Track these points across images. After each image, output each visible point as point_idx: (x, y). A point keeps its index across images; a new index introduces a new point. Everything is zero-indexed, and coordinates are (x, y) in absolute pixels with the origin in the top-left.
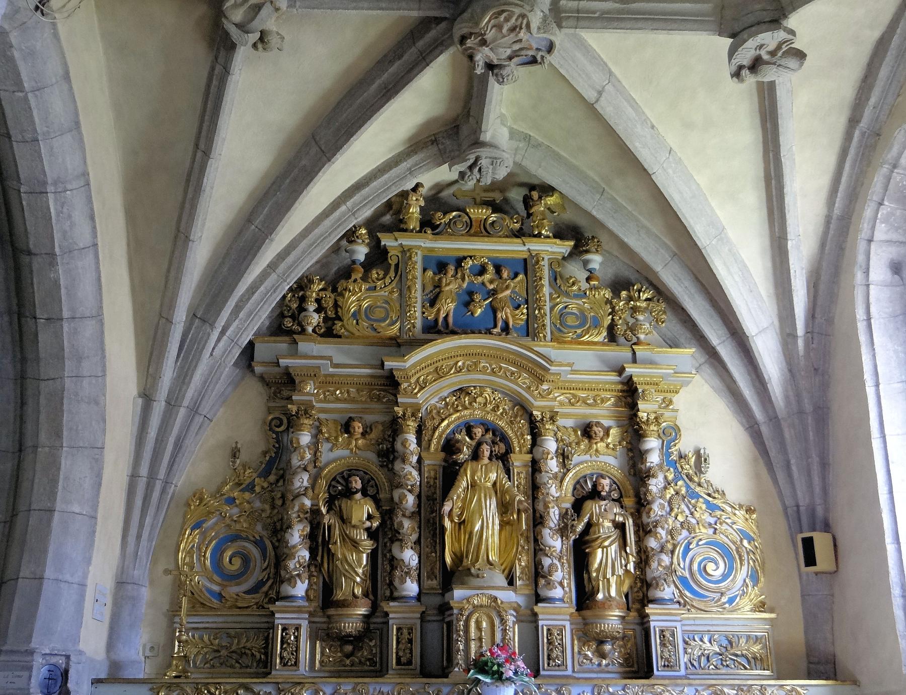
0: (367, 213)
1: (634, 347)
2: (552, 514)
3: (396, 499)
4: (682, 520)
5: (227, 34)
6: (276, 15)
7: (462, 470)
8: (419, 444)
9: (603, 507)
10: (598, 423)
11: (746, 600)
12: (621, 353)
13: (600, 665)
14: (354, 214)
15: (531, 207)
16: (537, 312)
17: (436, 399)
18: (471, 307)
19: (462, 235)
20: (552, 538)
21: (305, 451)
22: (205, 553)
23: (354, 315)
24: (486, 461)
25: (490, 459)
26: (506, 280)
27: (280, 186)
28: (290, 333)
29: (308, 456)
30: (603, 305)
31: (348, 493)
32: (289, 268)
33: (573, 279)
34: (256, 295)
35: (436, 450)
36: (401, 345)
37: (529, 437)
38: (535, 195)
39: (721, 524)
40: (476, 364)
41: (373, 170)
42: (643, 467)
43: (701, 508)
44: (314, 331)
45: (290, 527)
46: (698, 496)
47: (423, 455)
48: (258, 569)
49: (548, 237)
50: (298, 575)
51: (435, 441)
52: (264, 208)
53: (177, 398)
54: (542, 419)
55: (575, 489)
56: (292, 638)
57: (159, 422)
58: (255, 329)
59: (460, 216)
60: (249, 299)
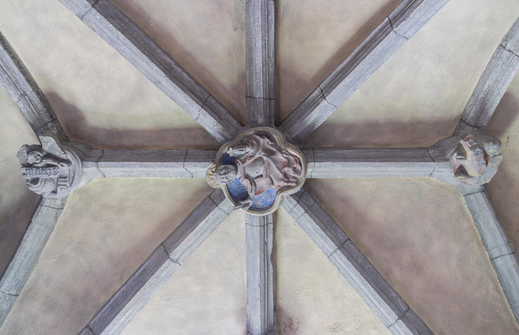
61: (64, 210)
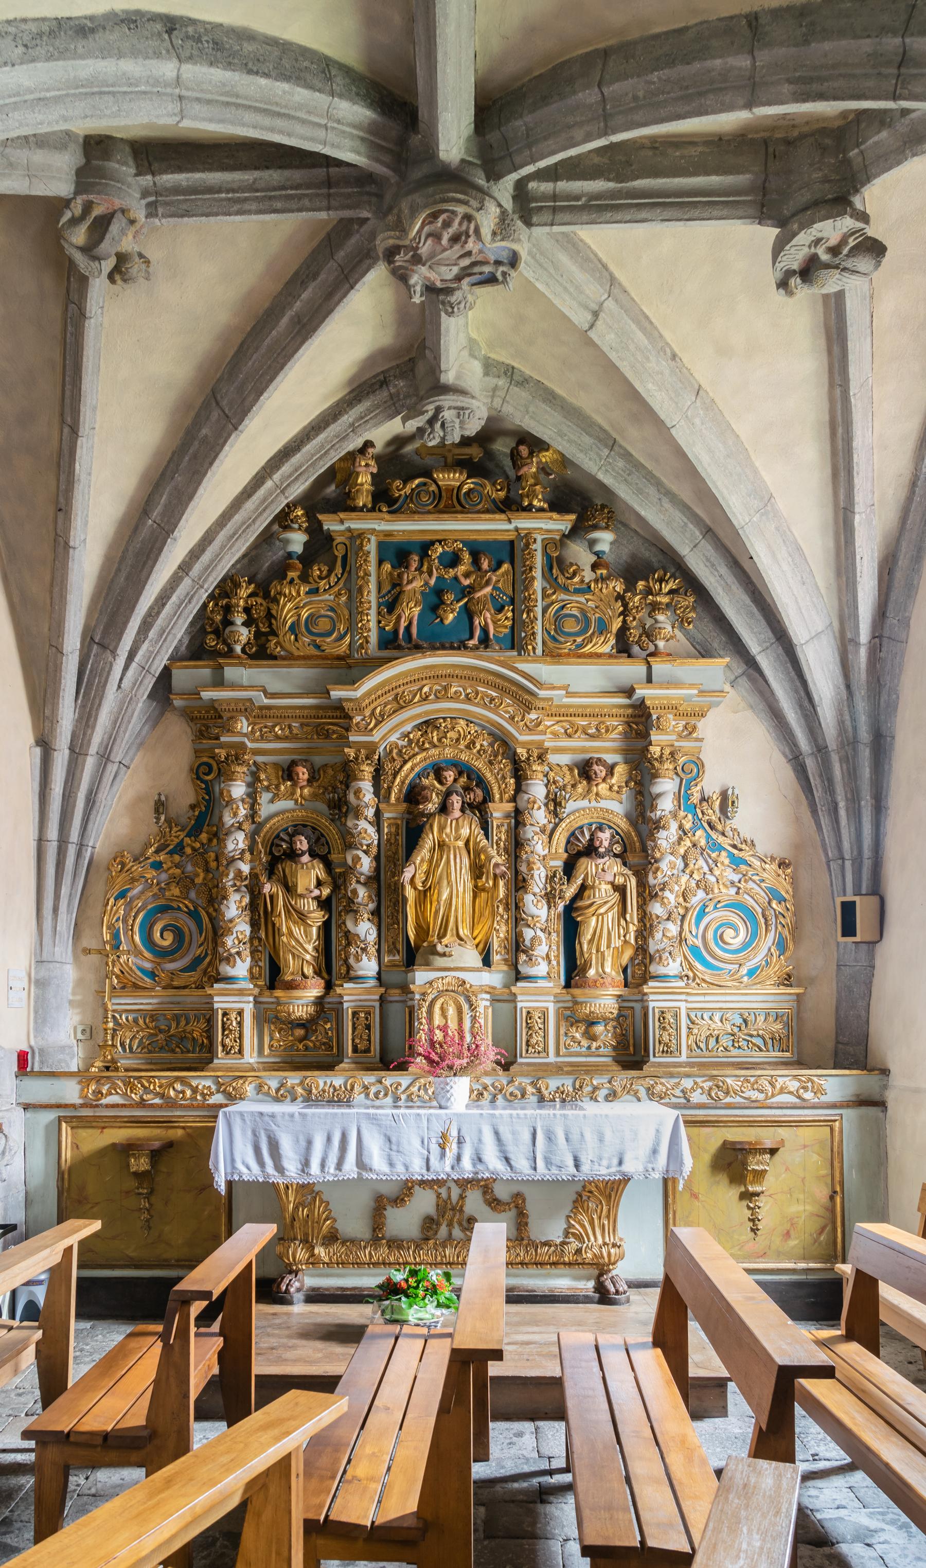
0: (298, 490)
1: (649, 659)
2: (536, 877)
3: (350, 862)
4: (697, 878)
5: (71, 263)
6: (133, 229)
7: (428, 826)
8: (376, 793)
9: (601, 867)
10: (599, 759)
11: (771, 971)
12: (630, 671)
13: (589, 1048)
14: (283, 492)
15: (519, 468)
16: (525, 616)
17: (397, 735)
18: (441, 612)
19: (429, 512)
20: (536, 906)
21: (238, 808)
22: (132, 926)
23: (293, 629)
24: (457, 813)
25: (462, 810)
26: (487, 572)
27: (178, 465)
28: (215, 654)
29: (242, 812)
30: (613, 600)
31: (292, 855)
32: (206, 569)
33: (575, 567)
34: (167, 607)
35: (397, 799)
36: (351, 668)
37: (512, 781)
38: (524, 450)
39: (746, 881)
40: (446, 688)
41: (305, 428)
42: (653, 815)
43: (722, 863)
44: (243, 650)
45: (225, 898)
46: (721, 848)
47: (382, 806)
48: (194, 945)
49: (541, 510)
50: (238, 953)
51: (395, 789)
52: (161, 496)
53: (82, 744)
54: (528, 759)
55: (568, 842)
56: (234, 1024)
57: (64, 775)
58: (170, 651)
59: (425, 484)
60: (158, 613)
61: (516, 365)
